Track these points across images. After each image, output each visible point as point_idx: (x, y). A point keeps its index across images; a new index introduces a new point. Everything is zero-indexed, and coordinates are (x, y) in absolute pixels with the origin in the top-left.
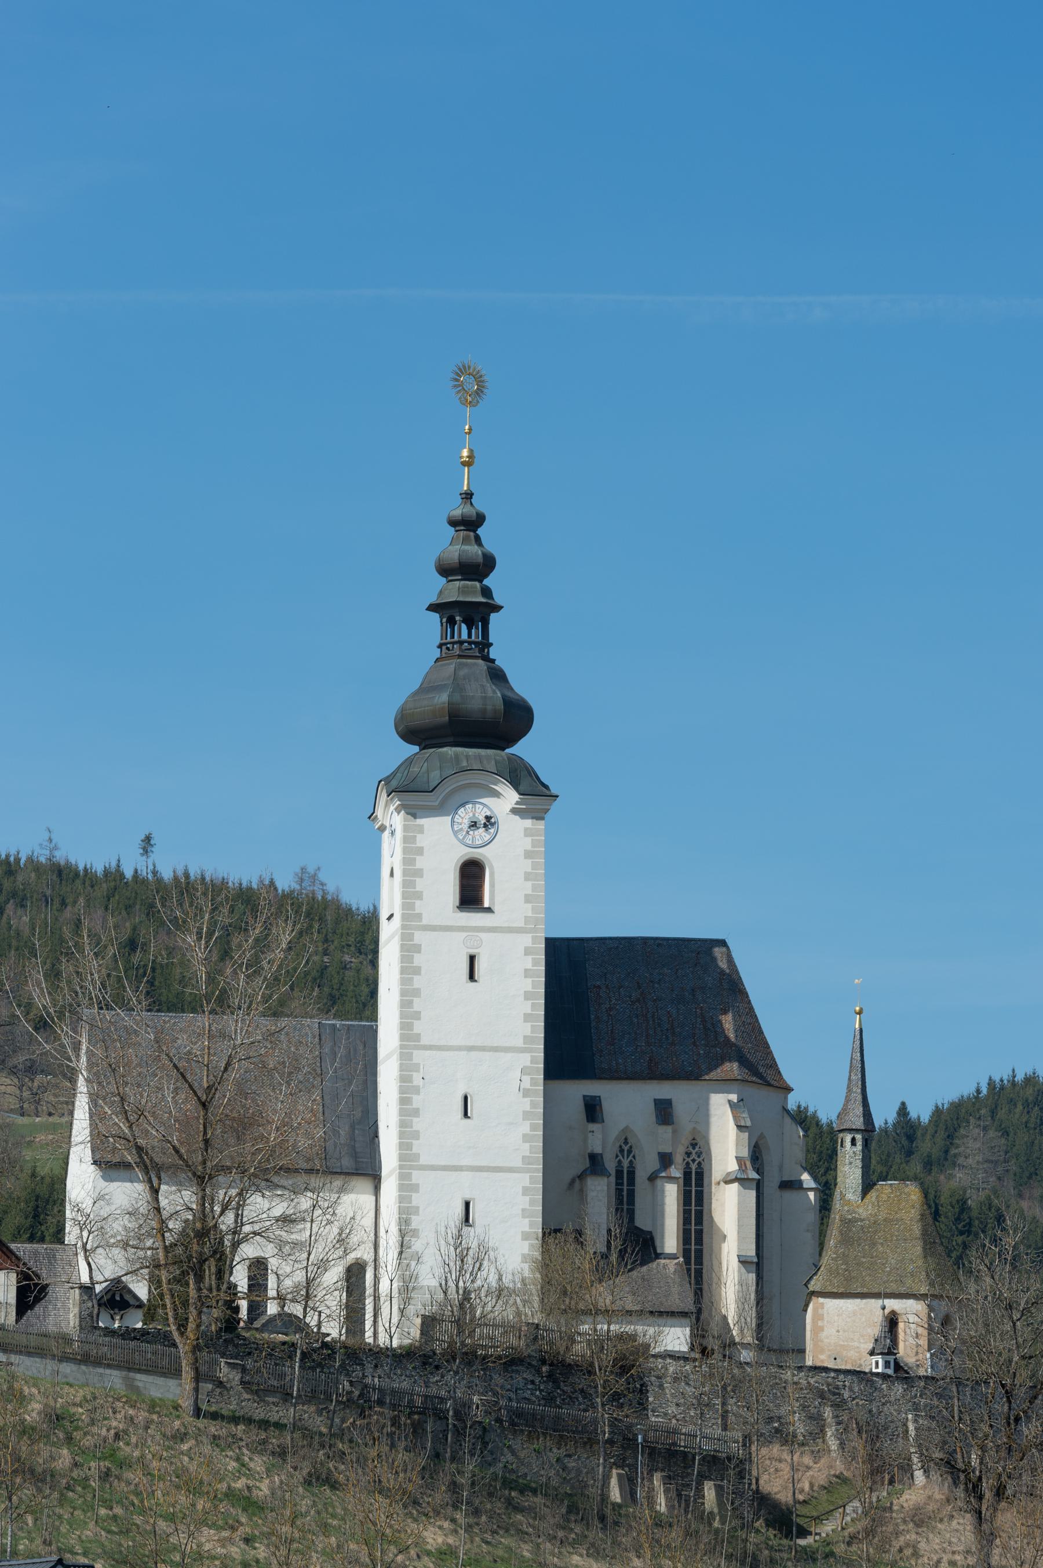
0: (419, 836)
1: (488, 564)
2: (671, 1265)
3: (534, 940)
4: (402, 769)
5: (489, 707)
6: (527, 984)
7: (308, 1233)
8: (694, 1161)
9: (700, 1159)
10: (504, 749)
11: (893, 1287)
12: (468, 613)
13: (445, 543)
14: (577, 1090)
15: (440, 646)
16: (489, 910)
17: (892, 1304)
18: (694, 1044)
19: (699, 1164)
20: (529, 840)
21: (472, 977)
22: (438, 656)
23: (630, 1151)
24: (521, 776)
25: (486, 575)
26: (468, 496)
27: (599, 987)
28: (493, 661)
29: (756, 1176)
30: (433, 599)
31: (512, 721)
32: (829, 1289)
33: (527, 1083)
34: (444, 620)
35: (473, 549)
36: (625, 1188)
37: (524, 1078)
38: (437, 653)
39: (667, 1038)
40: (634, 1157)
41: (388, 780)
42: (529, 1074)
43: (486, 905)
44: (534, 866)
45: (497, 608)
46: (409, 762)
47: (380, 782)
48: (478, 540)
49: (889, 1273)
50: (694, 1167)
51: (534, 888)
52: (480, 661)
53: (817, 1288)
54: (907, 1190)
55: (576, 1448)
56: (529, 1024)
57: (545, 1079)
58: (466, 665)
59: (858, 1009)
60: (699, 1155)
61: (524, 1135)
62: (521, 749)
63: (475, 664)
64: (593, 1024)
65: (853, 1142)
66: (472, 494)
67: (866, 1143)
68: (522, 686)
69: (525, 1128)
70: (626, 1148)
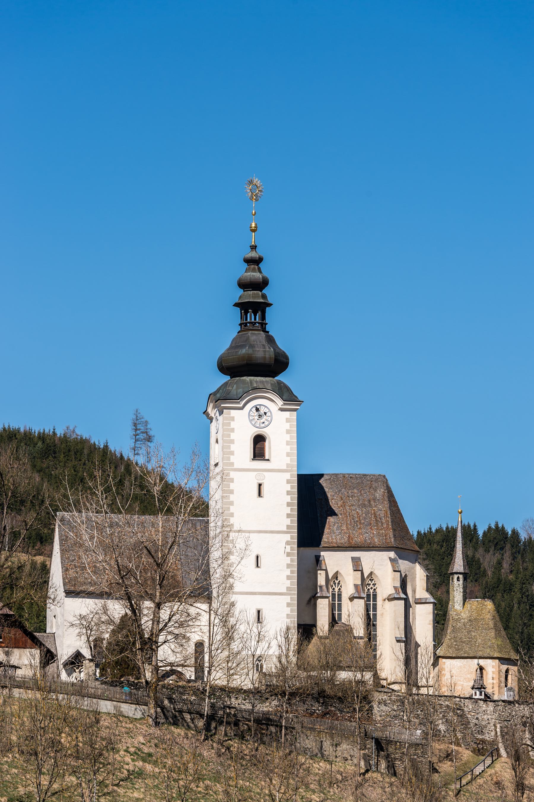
2: (361, 642)
3: (292, 476)
4: (222, 388)
5: (267, 356)
7: (493, 733)
8: (372, 588)
9: (375, 588)
10: (274, 377)
11: (480, 654)
12: (253, 308)
13: (242, 271)
14: (310, 552)
15: (241, 325)
16: (268, 460)
17: (482, 662)
18: (371, 528)
19: (375, 590)
21: (260, 495)
22: (240, 330)
23: (339, 583)
24: (288, 396)
25: (264, 288)
27: (321, 499)
28: (268, 332)
29: (405, 597)
30: (237, 301)
31: (277, 365)
32: (448, 655)
33: (288, 548)
34: (243, 311)
39: (357, 526)
40: (341, 586)
41: (215, 394)
42: (289, 545)
43: (267, 458)
45: (270, 305)
46: (226, 384)
47: (210, 395)
48: (260, 271)
49: (478, 646)
50: (371, 591)
52: (262, 332)
53: (441, 655)
54: (485, 603)
55: (342, 740)
56: (289, 519)
57: (299, 546)
58: (255, 334)
59: (460, 510)
63: (259, 334)
64: (319, 518)
65: (458, 579)
66: (256, 246)
67: (465, 579)
69: (288, 572)
70: (337, 582)
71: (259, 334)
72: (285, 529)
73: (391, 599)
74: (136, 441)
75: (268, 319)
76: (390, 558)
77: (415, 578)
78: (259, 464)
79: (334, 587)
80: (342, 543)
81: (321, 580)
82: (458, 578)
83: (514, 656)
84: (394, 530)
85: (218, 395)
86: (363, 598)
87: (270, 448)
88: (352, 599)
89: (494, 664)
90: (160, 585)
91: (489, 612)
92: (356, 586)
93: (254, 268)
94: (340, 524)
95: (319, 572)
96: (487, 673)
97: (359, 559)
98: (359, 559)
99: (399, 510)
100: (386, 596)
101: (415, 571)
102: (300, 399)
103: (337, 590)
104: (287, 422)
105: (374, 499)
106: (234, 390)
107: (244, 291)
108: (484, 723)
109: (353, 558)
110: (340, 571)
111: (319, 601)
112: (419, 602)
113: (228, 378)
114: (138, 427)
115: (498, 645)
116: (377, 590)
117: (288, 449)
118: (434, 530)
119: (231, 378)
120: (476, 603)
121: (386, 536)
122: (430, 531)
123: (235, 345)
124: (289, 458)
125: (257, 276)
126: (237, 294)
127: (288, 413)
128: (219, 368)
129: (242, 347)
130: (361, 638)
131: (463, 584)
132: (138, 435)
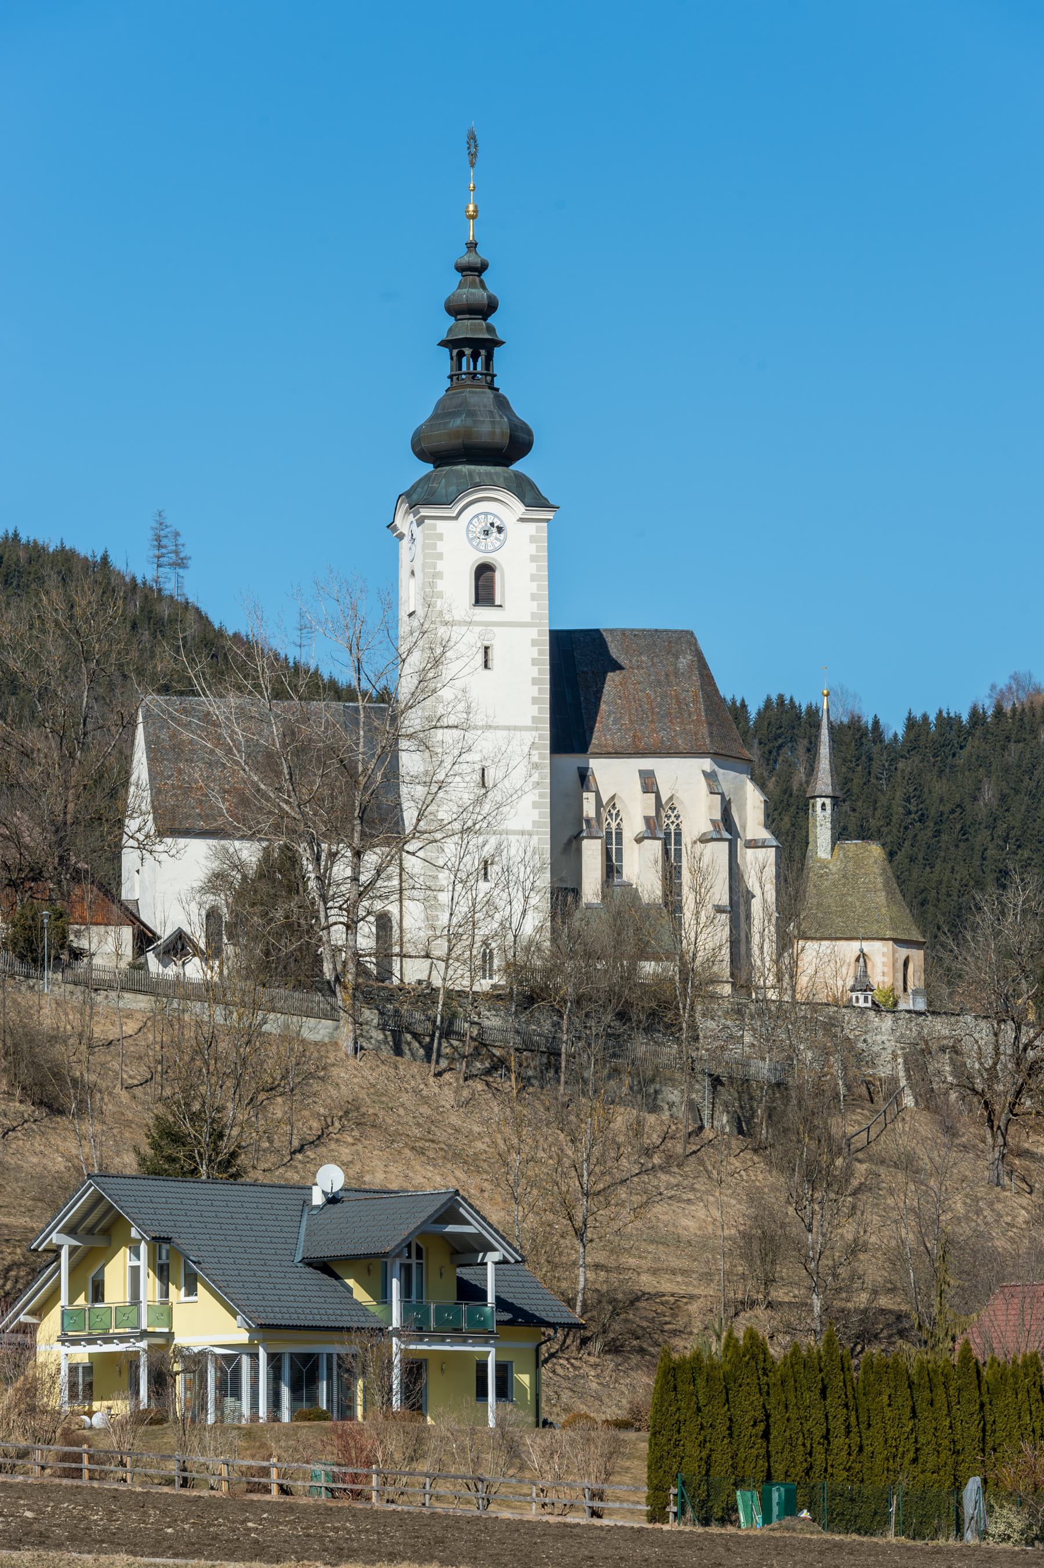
0: (439, 543)
1: (491, 307)
3: (540, 633)
6: (534, 672)
10: (508, 466)
12: (473, 346)
14: (571, 761)
15: (451, 377)
17: (868, 946)
18: (670, 721)
19: (678, 825)
20: (534, 546)
23: (617, 815)
24: (530, 495)
28: (497, 390)
30: (444, 336)
31: (517, 444)
36: (614, 847)
37: (533, 752)
39: (647, 717)
41: (408, 494)
44: (539, 568)
45: (500, 343)
46: (427, 478)
50: (673, 827)
51: (539, 587)
59: (825, 692)
60: (677, 817)
61: (534, 803)
62: (518, 466)
64: (583, 705)
68: (522, 411)
70: (614, 812)
71: (483, 392)
73: (704, 840)
74: (159, 566)
75: (497, 366)
76: (703, 772)
77: (746, 804)
78: (485, 613)
79: (609, 820)
80: (623, 747)
81: (589, 809)
82: (823, 805)
83: (916, 936)
84: (710, 724)
85: (415, 497)
86: (659, 839)
87: (503, 586)
88: (639, 840)
89: (885, 950)
90: (361, 818)
91: (875, 862)
92: (647, 819)
93: (474, 281)
94: (619, 715)
95: (585, 795)
96: (873, 966)
100: (696, 835)
101: (745, 793)
102: (552, 502)
103: (614, 825)
104: (531, 542)
105: (676, 672)
106: (441, 487)
107: (456, 320)
108: (876, 1049)
110: (619, 794)
111: (586, 844)
112: (752, 844)
113: (429, 468)
114: (163, 543)
115: (891, 918)
116: (682, 826)
117: (533, 587)
119: (436, 467)
120: (853, 848)
121: (696, 734)
123: (443, 412)
124: (535, 603)
125: (478, 295)
127: (533, 526)
128: (415, 453)
129: (454, 414)
131: (832, 815)
132: (163, 556)
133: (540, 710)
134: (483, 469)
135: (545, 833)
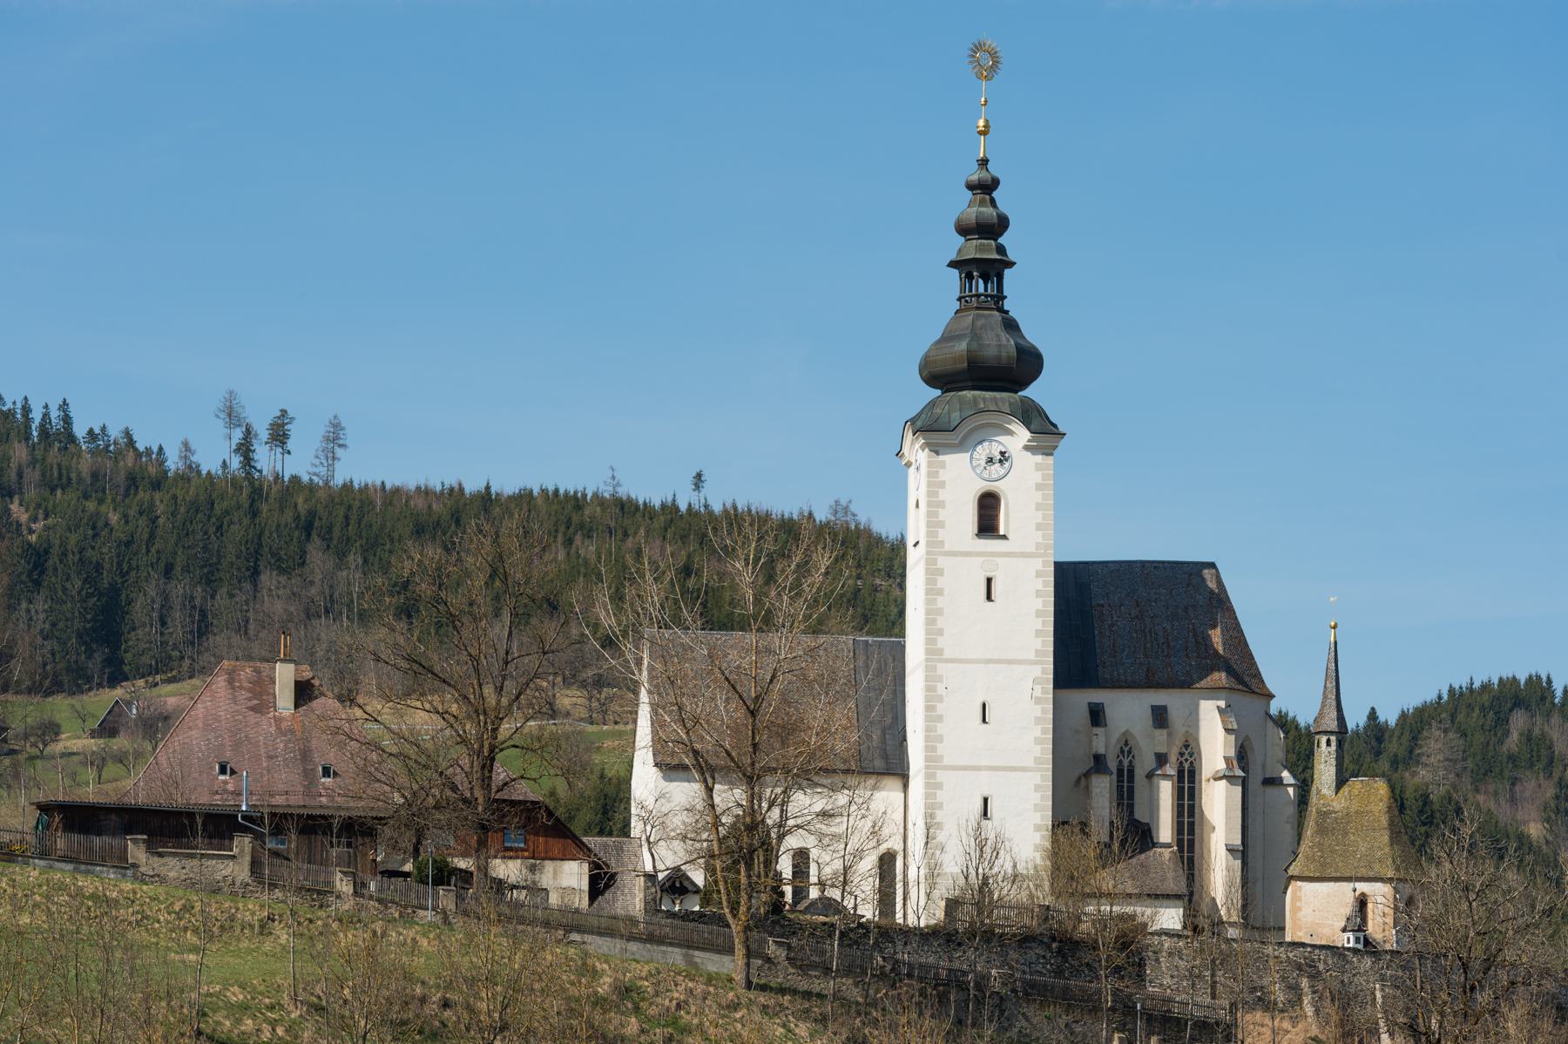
1: (1002, 224)
2: (1167, 853)
11: (1363, 872)
12: (984, 271)
13: (962, 204)
14: (1082, 698)
15: (959, 299)
16: (1004, 537)
17: (1362, 887)
21: (989, 598)
25: (1001, 234)
26: (984, 163)
28: (1007, 312)
29: (1242, 774)
30: (953, 256)
31: (1027, 365)
32: (1307, 874)
35: (988, 211)
38: (957, 306)
41: (913, 421)
45: (1011, 264)
48: (993, 202)
53: (1296, 873)
65: (1328, 743)
67: (1340, 744)
68: (1033, 334)
72: (1032, 656)
87: (1007, 515)
97: (1164, 708)
98: (1164, 708)
99: (1238, 624)
102: (1062, 430)
109: (1154, 708)
113: (938, 392)
118: (1477, 685)
120: (1359, 785)
122: (1471, 690)
126: (954, 245)
130: (1168, 846)
133: (1043, 798)
134: (988, 394)
135: (1046, 663)
